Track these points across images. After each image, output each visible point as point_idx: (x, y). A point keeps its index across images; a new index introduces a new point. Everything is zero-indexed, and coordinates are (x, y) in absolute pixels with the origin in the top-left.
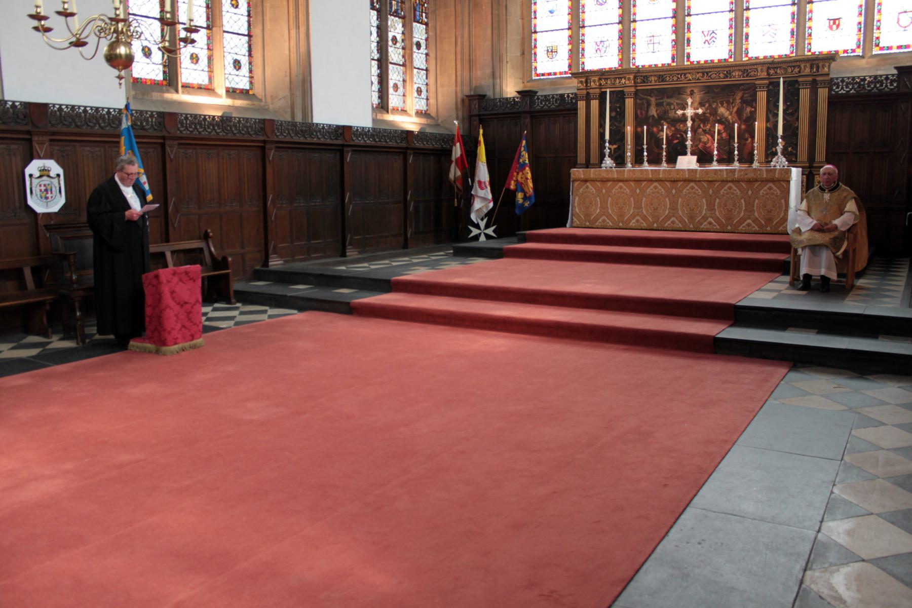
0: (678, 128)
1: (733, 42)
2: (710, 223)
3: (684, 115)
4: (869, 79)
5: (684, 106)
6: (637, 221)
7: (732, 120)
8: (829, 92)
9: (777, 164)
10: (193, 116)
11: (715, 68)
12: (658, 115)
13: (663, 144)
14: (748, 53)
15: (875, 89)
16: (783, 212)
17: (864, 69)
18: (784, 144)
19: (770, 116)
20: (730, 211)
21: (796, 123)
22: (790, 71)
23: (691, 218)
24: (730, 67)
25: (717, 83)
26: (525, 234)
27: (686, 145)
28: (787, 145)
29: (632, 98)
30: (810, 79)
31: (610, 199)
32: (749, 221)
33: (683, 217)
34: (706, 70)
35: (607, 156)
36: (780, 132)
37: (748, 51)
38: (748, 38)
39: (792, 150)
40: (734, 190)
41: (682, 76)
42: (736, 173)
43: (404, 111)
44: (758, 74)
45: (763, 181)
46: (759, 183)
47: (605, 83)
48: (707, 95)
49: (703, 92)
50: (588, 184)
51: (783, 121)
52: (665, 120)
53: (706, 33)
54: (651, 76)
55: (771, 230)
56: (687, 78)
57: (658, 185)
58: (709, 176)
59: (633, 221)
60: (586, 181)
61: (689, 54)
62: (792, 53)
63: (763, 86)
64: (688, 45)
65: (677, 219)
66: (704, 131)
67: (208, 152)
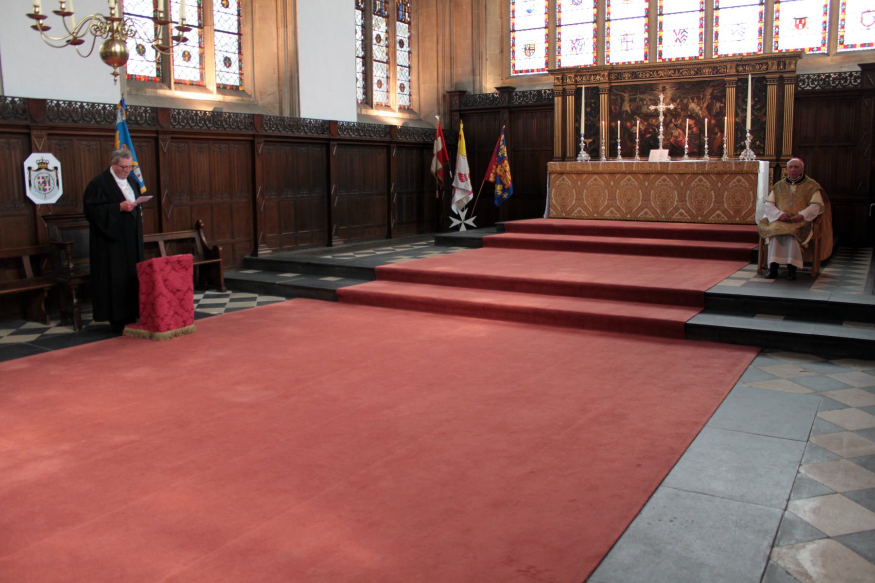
0: (651, 123)
1: (703, 40)
2: (681, 214)
3: (656, 110)
4: (834, 76)
5: (656, 101)
6: (612, 212)
7: (702, 115)
8: (796, 88)
9: (746, 158)
10: (185, 111)
11: (686, 65)
12: (631, 110)
13: (636, 138)
14: (717, 51)
15: (839, 85)
16: (751, 203)
17: (829, 66)
18: (752, 138)
19: (739, 111)
20: (700, 202)
21: (763, 118)
22: (758, 68)
23: (663, 209)
24: (701, 64)
25: (688, 80)
26: (503, 225)
27: (658, 139)
28: (755, 139)
29: (606, 93)
30: (777, 75)
31: (585, 191)
32: (718, 212)
33: (656, 209)
34: (678, 67)
35: (582, 150)
36: (749, 126)
37: (717, 49)
38: (717, 37)
39: (760, 144)
40: (704, 182)
41: (655, 73)
42: (707, 166)
43: (387, 106)
44: (728, 71)
45: (732, 173)
46: (729, 175)
47: (580, 79)
48: (678, 91)
49: (675, 88)
50: (564, 176)
51: (752, 116)
52: (638, 115)
53: (677, 32)
54: (625, 72)
55: (740, 220)
56: (659, 75)
57: (631, 178)
58: (680, 168)
59: (608, 212)
60: (562, 174)
61: (661, 52)
62: (760, 50)
63: (732, 83)
64: (661, 43)
65: (649, 210)
66: (676, 126)
67: (200, 146)
